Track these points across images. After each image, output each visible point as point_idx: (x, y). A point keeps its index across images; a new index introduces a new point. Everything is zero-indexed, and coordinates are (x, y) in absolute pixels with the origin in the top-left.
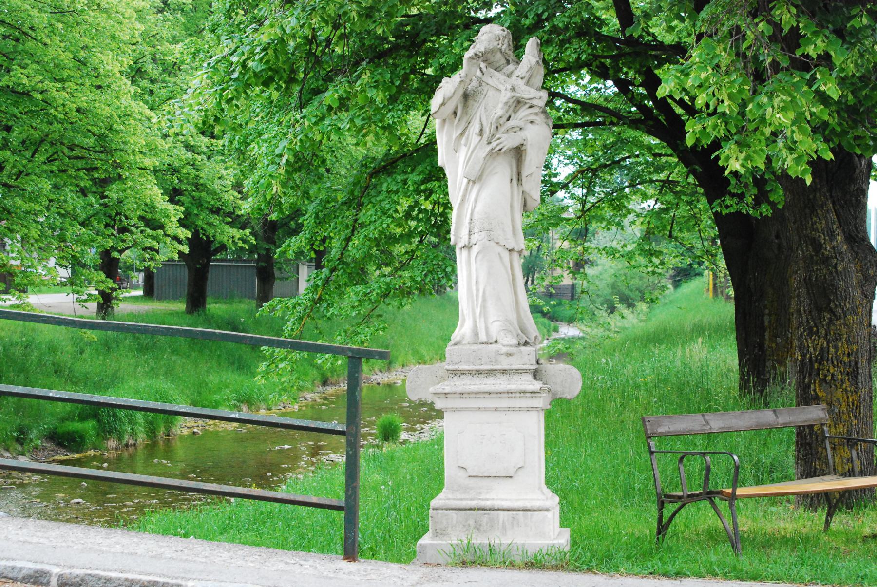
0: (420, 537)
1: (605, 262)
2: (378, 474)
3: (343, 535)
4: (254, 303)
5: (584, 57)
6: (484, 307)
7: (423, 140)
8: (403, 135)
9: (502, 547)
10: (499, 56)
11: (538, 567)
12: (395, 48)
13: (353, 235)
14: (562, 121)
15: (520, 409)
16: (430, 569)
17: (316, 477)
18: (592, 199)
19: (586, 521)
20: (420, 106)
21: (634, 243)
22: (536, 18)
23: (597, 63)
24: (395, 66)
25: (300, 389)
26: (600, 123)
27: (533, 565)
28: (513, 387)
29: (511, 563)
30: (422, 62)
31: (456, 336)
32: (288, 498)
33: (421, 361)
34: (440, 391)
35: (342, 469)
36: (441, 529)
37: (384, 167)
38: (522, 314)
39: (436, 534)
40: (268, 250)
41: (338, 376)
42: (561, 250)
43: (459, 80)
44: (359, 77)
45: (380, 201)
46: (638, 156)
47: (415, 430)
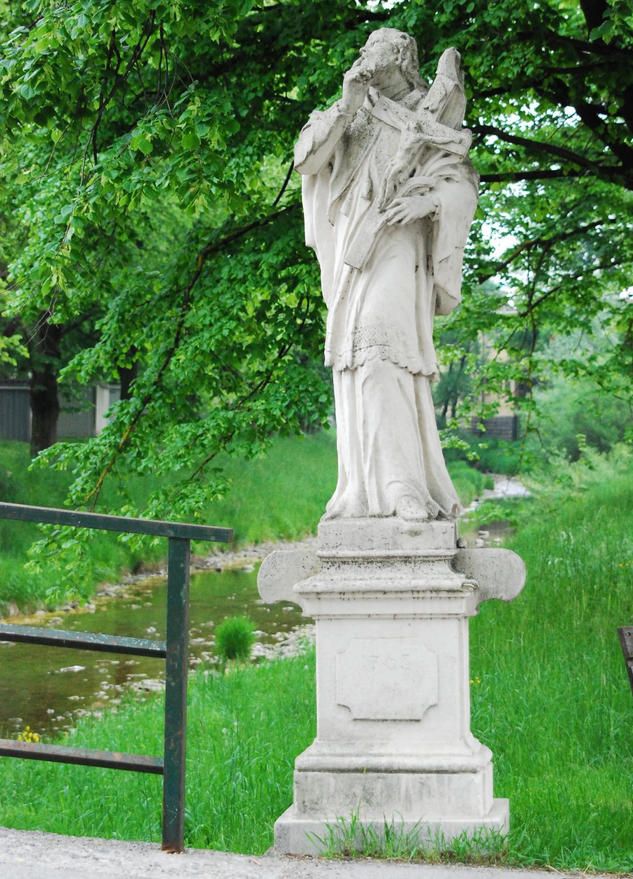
0: (280, 812)
1: (562, 380)
2: (218, 710)
3: (161, 810)
4: (27, 448)
5: (529, 71)
6: (376, 462)
7: (284, 200)
8: (253, 192)
9: (405, 829)
10: (397, 76)
11: (461, 860)
12: (240, 58)
13: (177, 346)
14: (496, 169)
15: (431, 617)
16: (294, 863)
17: (119, 720)
18: (543, 288)
19: (535, 787)
20: (279, 149)
21: (608, 351)
22: (456, 12)
23: (551, 79)
24: (241, 86)
25: (99, 578)
26: (554, 174)
27: (453, 856)
28: (421, 583)
29: (419, 853)
30: (282, 80)
31: (333, 505)
32: (77, 756)
33: (285, 535)
34: (310, 588)
35: (161, 702)
36: (312, 802)
37: (225, 242)
38: (434, 471)
39: (304, 809)
40: (49, 367)
41: (157, 558)
42: (496, 366)
43: (337, 114)
44: (183, 108)
45: (218, 294)
46: (613, 221)
47: (274, 641)
